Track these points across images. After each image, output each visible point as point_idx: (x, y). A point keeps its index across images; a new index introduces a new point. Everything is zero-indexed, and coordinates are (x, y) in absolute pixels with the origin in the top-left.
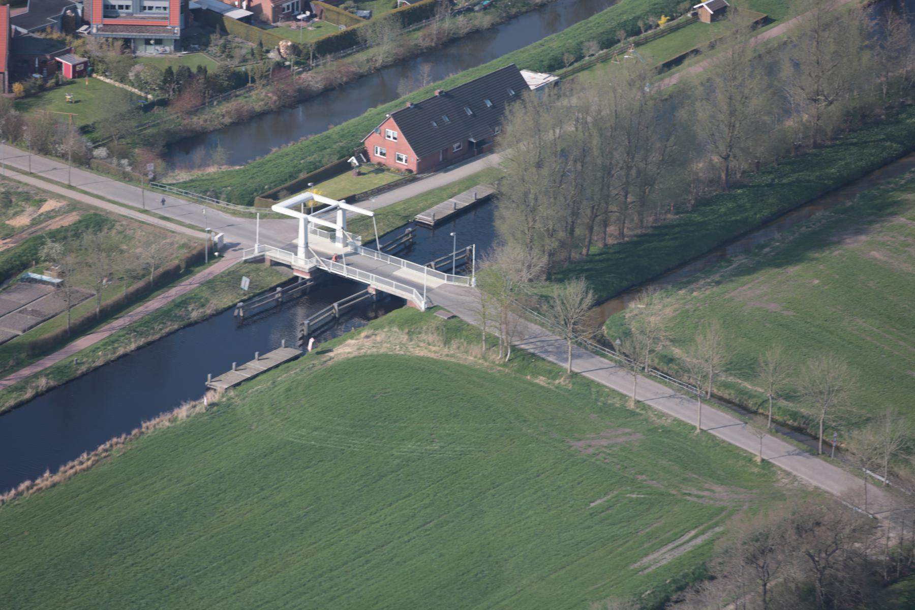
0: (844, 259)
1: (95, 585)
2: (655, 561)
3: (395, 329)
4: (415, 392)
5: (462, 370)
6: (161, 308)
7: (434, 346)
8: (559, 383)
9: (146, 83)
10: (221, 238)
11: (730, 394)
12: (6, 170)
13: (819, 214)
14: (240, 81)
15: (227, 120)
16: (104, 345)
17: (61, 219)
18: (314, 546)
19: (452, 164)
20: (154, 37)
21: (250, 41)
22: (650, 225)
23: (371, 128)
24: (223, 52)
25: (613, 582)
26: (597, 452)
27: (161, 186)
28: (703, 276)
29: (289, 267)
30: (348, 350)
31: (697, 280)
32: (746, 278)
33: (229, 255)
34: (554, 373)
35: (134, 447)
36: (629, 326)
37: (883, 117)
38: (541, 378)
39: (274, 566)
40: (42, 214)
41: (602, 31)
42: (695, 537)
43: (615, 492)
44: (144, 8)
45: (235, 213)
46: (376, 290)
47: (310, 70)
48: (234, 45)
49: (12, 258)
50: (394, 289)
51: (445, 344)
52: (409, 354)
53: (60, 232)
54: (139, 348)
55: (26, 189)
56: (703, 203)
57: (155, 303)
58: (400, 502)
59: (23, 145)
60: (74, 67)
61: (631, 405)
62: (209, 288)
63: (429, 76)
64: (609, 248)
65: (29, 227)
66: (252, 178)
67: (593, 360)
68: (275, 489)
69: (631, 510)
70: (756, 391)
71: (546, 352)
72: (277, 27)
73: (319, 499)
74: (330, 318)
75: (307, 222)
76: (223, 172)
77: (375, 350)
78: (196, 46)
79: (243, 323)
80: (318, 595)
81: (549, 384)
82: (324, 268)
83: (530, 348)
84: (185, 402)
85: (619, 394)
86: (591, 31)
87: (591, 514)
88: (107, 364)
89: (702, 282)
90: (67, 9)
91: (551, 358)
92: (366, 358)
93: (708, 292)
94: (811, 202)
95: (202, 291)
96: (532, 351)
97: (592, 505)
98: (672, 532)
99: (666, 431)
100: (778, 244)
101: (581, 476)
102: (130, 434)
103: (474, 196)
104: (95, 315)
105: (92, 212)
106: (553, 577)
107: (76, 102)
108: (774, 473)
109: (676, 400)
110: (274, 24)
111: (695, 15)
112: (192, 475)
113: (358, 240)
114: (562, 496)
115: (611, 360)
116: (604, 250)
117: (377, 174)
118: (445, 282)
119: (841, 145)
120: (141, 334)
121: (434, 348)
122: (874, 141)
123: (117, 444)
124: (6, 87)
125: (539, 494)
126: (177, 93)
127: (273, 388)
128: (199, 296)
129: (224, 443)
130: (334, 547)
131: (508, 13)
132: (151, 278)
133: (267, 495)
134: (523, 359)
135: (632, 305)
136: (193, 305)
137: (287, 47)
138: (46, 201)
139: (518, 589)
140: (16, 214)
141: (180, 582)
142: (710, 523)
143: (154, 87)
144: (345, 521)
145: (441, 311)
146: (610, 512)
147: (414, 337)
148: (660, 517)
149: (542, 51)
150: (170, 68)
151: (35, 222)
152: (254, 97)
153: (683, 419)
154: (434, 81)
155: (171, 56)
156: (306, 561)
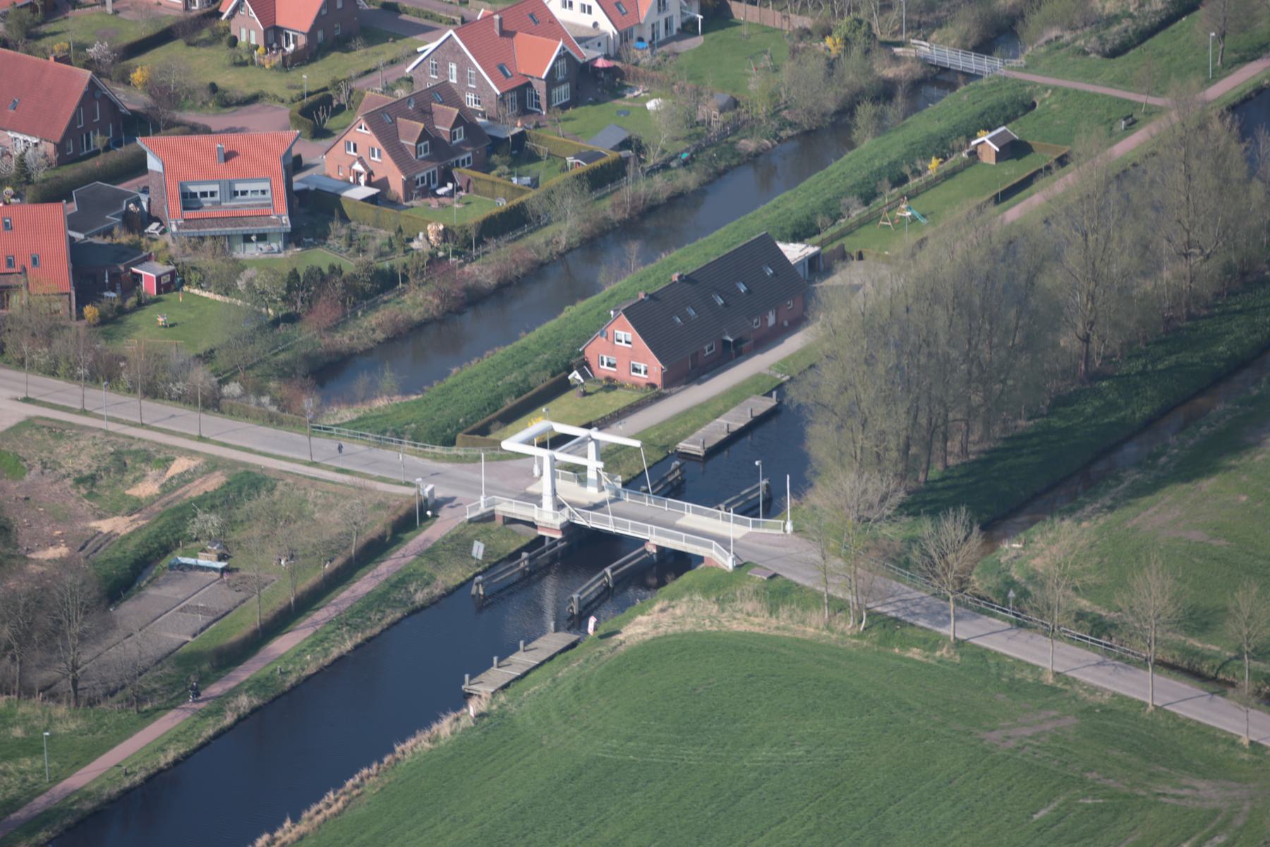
3: (697, 597)
5: (800, 645)
6: (373, 590)
8: (942, 655)
9: (263, 293)
10: (432, 492)
12: (109, 423)
13: (1220, 407)
14: (387, 282)
15: (380, 336)
16: (311, 645)
17: (202, 483)
22: (998, 435)
23: (599, 324)
24: (350, 246)
26: (1020, 745)
27: (324, 429)
28: (1088, 500)
29: (532, 525)
30: (640, 630)
31: (1082, 506)
32: (1146, 500)
33: (445, 513)
34: (931, 642)
35: (392, 779)
36: (1008, 574)
38: (915, 650)
40: (173, 477)
41: (852, 184)
43: (1062, 799)
44: (236, 193)
45: (435, 458)
46: (658, 547)
47: (473, 261)
48: (361, 235)
49: (147, 539)
50: (684, 544)
51: (771, 614)
52: (724, 629)
53: (205, 500)
54: (357, 647)
55: (142, 446)
56: (1060, 401)
57: (364, 585)
59: (121, 387)
60: (158, 278)
61: (1050, 680)
62: (431, 559)
63: (638, 257)
64: (952, 471)
65: (160, 496)
66: (439, 409)
67: (978, 622)
70: (1209, 650)
71: (913, 614)
72: (412, 207)
74: (602, 589)
75: (553, 460)
77: (677, 628)
78: (311, 240)
79: (483, 604)
81: (927, 657)
82: (580, 521)
83: (890, 611)
84: (445, 714)
85: (1028, 664)
86: (838, 184)
87: (1038, 830)
88: (321, 671)
89: (1089, 509)
90: (128, 203)
91: (921, 623)
93: (1101, 521)
94: (1201, 392)
96: (894, 614)
97: (1036, 817)
99: (1106, 711)
100: (1176, 451)
101: (1009, 779)
102: (382, 762)
105: (241, 469)
107: (171, 326)
109: (1107, 667)
110: (408, 204)
111: (974, 153)
113: (617, 482)
116: (946, 473)
118: (750, 529)
120: (355, 628)
121: (757, 620)
123: (368, 776)
127: (558, 685)
128: (420, 571)
129: (511, 766)
131: (715, 168)
132: (353, 551)
134: (884, 626)
135: (1005, 546)
136: (414, 584)
138: (173, 460)
142: (1206, 831)
146: (1062, 825)
147: (727, 606)
148: (1135, 828)
149: (779, 215)
150: (295, 270)
151: (166, 489)
152: (409, 302)
154: (644, 264)
155: (282, 255)
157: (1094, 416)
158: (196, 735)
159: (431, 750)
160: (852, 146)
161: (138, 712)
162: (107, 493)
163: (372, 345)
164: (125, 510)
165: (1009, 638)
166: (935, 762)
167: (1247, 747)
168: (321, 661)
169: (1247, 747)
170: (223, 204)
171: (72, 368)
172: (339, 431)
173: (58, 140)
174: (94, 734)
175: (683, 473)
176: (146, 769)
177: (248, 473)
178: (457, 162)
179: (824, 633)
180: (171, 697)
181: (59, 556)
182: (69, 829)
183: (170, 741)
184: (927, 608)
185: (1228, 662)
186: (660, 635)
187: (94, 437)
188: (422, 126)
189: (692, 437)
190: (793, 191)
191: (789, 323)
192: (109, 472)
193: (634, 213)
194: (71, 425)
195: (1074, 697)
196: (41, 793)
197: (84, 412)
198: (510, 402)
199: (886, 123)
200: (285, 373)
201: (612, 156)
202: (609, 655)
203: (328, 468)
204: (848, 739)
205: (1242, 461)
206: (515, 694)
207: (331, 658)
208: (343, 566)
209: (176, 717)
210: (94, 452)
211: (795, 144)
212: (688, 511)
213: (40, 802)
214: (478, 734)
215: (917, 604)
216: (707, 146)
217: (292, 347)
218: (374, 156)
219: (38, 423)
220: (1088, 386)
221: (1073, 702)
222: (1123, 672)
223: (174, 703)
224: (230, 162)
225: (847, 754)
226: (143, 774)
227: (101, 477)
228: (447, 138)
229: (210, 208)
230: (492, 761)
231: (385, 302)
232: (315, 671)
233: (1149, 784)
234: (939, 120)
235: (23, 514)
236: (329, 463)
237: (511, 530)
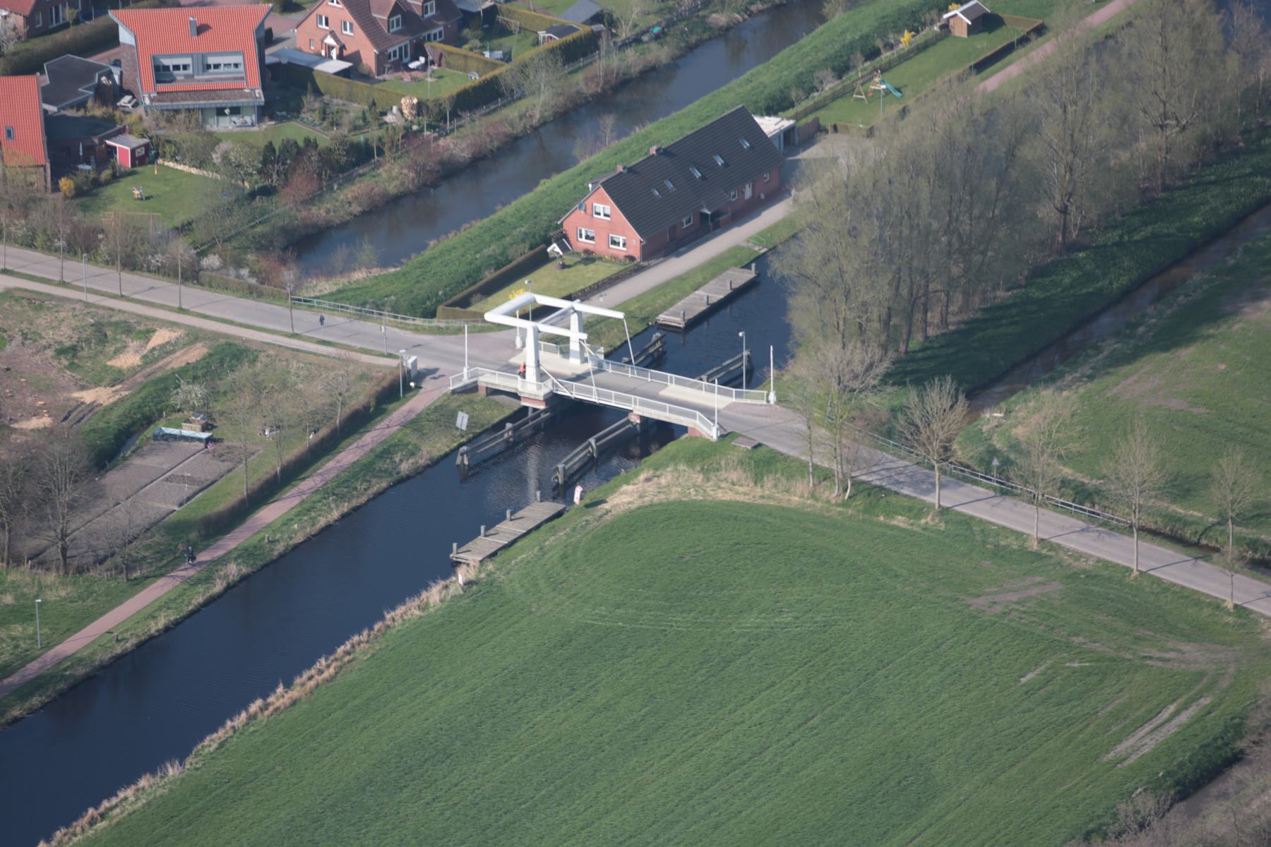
0: (1250, 334)
1: (393, 829)
2: (1135, 749)
3: (682, 467)
4: (735, 548)
5: (787, 515)
6: (358, 460)
7: (742, 485)
8: (927, 523)
10: (414, 363)
11: (1156, 523)
14: (363, 155)
15: (356, 209)
16: (298, 515)
17: (183, 354)
18: (667, 759)
19: (683, 245)
20: (230, 105)
21: (356, 102)
23: (578, 197)
24: (324, 119)
25: (1086, 781)
27: (305, 301)
28: (1068, 369)
29: (515, 396)
30: (626, 499)
31: (1062, 375)
32: (1126, 369)
33: (428, 384)
34: (917, 510)
35: (383, 646)
37: (1241, 144)
38: (900, 517)
39: (624, 789)
40: (154, 349)
42: (1177, 713)
43: (1049, 663)
44: (209, 67)
45: (417, 329)
46: (641, 417)
47: (447, 134)
49: (130, 411)
50: (668, 414)
51: (756, 483)
53: (187, 371)
55: (123, 318)
56: (1039, 272)
57: (349, 455)
58: (763, 693)
59: (99, 259)
60: (133, 151)
61: (1035, 546)
63: (612, 131)
64: (931, 342)
65: (142, 367)
66: (418, 282)
67: (962, 490)
68: (590, 687)
69: (1078, 684)
70: (1192, 516)
71: (898, 482)
72: (385, 81)
73: (653, 697)
74: (586, 459)
75: (537, 331)
76: (376, 278)
77: (662, 497)
78: (284, 113)
80: (696, 822)
81: (912, 525)
82: (564, 392)
83: (874, 479)
84: (435, 582)
85: (1013, 531)
86: (810, 58)
87: (1027, 693)
88: (308, 540)
89: (1069, 378)
90: (100, 76)
92: (655, 508)
93: (1082, 390)
95: (406, 435)
96: (878, 483)
97: (1023, 680)
98: (1143, 710)
99: (1091, 576)
102: (373, 629)
103: (728, 284)
104: (276, 475)
105: (223, 341)
106: (1002, 778)
107: (147, 198)
108: (1256, 622)
109: (1091, 534)
110: (380, 78)
111: (946, 27)
112: (473, 676)
114: (979, 671)
117: (586, 264)
118: (734, 400)
119: (1198, 184)
120: (342, 497)
121: (741, 489)
122: (1240, 177)
123: (359, 643)
124: (49, 185)
125: (948, 670)
126: (283, 176)
127: (543, 555)
128: (405, 442)
129: (500, 632)
130: (694, 759)
131: (687, 42)
133: (583, 696)
134: (869, 495)
136: (399, 454)
137: (412, 107)
138: (154, 331)
139: (962, 798)
140: (117, 352)
141: (505, 819)
143: (250, 170)
144: (699, 724)
145: (740, 438)
146: (1049, 688)
148: (1121, 690)
150: (271, 144)
151: (148, 360)
152: (384, 175)
153: (1109, 559)
155: (256, 128)
156: (665, 779)
158: (186, 603)
161: (128, 580)
163: (348, 218)
164: (108, 380)
165: (993, 506)
167: (1232, 611)
169: (1232, 611)
170: (196, 77)
171: (49, 239)
173: (27, 13)
174: (84, 601)
175: (664, 344)
176: (137, 636)
177: (230, 345)
178: (429, 36)
180: (160, 564)
182: (62, 694)
183: (160, 608)
184: (911, 477)
185: (1210, 527)
186: (646, 504)
187: (74, 309)
189: (671, 309)
190: (766, 65)
191: (766, 196)
192: (90, 343)
194: (51, 297)
195: (1059, 563)
196: (34, 659)
197: (63, 284)
198: (489, 275)
200: (263, 246)
201: (584, 30)
203: (310, 340)
204: (836, 606)
205: (1221, 330)
206: (503, 562)
209: (165, 585)
210: (74, 323)
212: (671, 382)
213: (33, 668)
214: (467, 601)
215: (900, 473)
218: (346, 29)
219: (18, 294)
220: (1066, 257)
221: (1058, 568)
222: (1106, 538)
223: (163, 571)
226: (134, 641)
227: (82, 348)
228: (419, 13)
229: (183, 81)
231: (360, 175)
232: (302, 540)
233: (1134, 647)
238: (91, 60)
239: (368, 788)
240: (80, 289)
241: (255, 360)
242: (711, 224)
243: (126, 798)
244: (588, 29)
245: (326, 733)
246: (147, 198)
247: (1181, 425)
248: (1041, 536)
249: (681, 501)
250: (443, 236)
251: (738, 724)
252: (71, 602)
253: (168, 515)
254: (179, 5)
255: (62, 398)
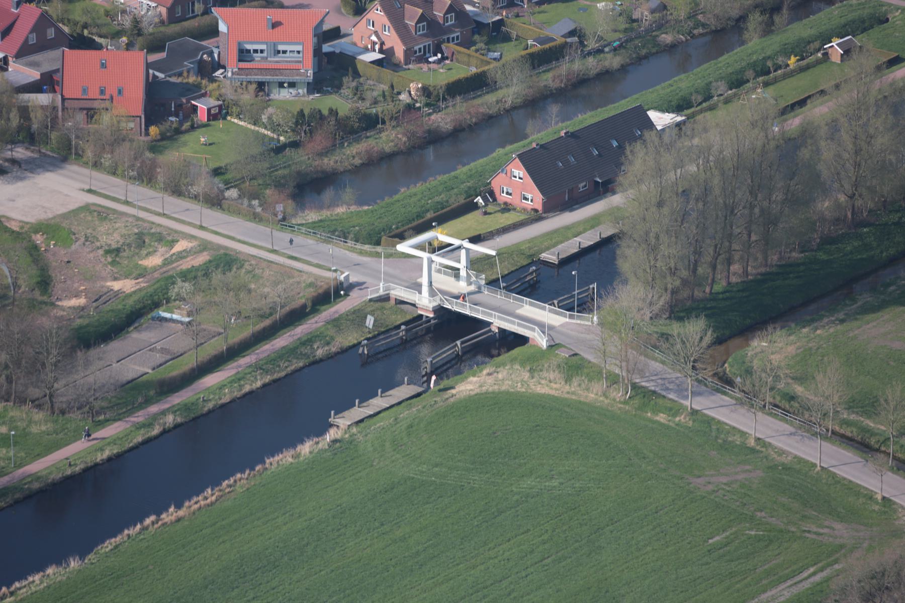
3: (517, 366)
7: (556, 383)
8: (680, 420)
10: (347, 278)
14: (370, 123)
15: (357, 161)
16: (231, 382)
18: (432, 581)
19: (577, 204)
20: (287, 81)
22: (774, 263)
23: (499, 167)
24: (355, 94)
26: (716, 489)
27: (289, 226)
28: (827, 314)
29: (414, 305)
30: (470, 387)
31: (821, 318)
33: (355, 294)
34: (674, 410)
38: (662, 415)
40: (174, 254)
42: (814, 574)
43: (734, 529)
44: (279, 52)
45: (361, 253)
46: (499, 328)
47: (440, 111)
49: (144, 297)
50: (516, 327)
51: (566, 382)
53: (191, 272)
54: (264, 386)
56: (828, 241)
57: (282, 341)
58: (519, 537)
59: (157, 186)
60: (209, 110)
61: (752, 443)
62: (334, 326)
63: (557, 116)
65: (161, 267)
66: (380, 218)
67: (713, 398)
68: (395, 524)
70: (878, 429)
71: (667, 389)
72: (409, 69)
74: (454, 356)
75: (431, 262)
77: (496, 387)
79: (367, 361)
83: (651, 386)
85: (740, 431)
86: (721, 71)
87: (709, 551)
88: (233, 401)
89: (826, 320)
93: (832, 330)
96: (653, 388)
97: (710, 541)
98: (790, 569)
99: (786, 468)
102: (254, 470)
104: (222, 352)
105: (222, 252)
107: (210, 144)
108: (895, 511)
110: (406, 67)
111: (826, 55)
114: (680, 532)
115: (731, 398)
117: (502, 213)
118: (567, 320)
120: (267, 372)
124: (143, 130)
125: (658, 529)
126: (309, 135)
127: (397, 423)
130: (452, 582)
131: (638, 54)
133: (388, 530)
134: (644, 396)
137: (418, 90)
138: (177, 241)
144: (464, 557)
145: (563, 349)
148: (779, 554)
150: (302, 111)
151: (167, 262)
153: (804, 456)
154: (563, 121)
155: (306, 99)
157: (851, 253)
159: (292, 463)
160: (743, 43)
161: (93, 421)
162: (126, 262)
164: (134, 275)
165: (732, 411)
166: (650, 498)
167: (880, 501)
168: (236, 393)
169: (880, 501)
170: (269, 59)
172: (300, 229)
173: (169, 5)
176: (86, 463)
177: (226, 255)
178: (448, 39)
179: (601, 398)
180: (121, 411)
181: (78, 305)
184: (678, 386)
187: (127, 221)
188: (421, 11)
190: (686, 74)
193: (569, 83)
194: (115, 211)
195: (766, 457)
197: (127, 203)
199: (773, 28)
201: (560, 41)
202: (442, 403)
207: (243, 392)
208: (269, 326)
210: (124, 231)
211: (707, 38)
214: (329, 454)
215: (672, 382)
216: (636, 38)
217: (289, 166)
218: (385, 31)
219: (93, 208)
221: (765, 460)
223: (122, 416)
224: (276, 29)
225: (588, 487)
226: (82, 466)
227: (124, 250)
228: (441, 22)
229: (259, 61)
230: (333, 475)
232: (228, 401)
233: (800, 523)
234: (811, 28)
235: (62, 273)
236: (285, 251)
237: (400, 308)
238: (204, 43)
239: (210, 586)
240: (134, 206)
241: (242, 267)
242: (601, 189)
243: (33, 582)
244: (563, 40)
245: (194, 544)
246: (210, 144)
247: (895, 361)
248: (759, 435)
249: (508, 392)
250: (412, 186)
251: (492, 559)
252: (48, 435)
253: (142, 376)
254: (282, 6)
255: (99, 285)
